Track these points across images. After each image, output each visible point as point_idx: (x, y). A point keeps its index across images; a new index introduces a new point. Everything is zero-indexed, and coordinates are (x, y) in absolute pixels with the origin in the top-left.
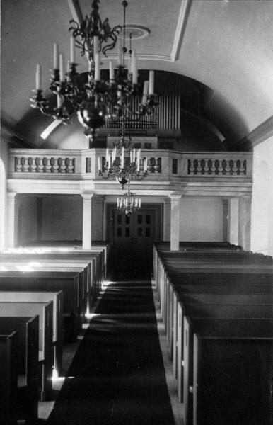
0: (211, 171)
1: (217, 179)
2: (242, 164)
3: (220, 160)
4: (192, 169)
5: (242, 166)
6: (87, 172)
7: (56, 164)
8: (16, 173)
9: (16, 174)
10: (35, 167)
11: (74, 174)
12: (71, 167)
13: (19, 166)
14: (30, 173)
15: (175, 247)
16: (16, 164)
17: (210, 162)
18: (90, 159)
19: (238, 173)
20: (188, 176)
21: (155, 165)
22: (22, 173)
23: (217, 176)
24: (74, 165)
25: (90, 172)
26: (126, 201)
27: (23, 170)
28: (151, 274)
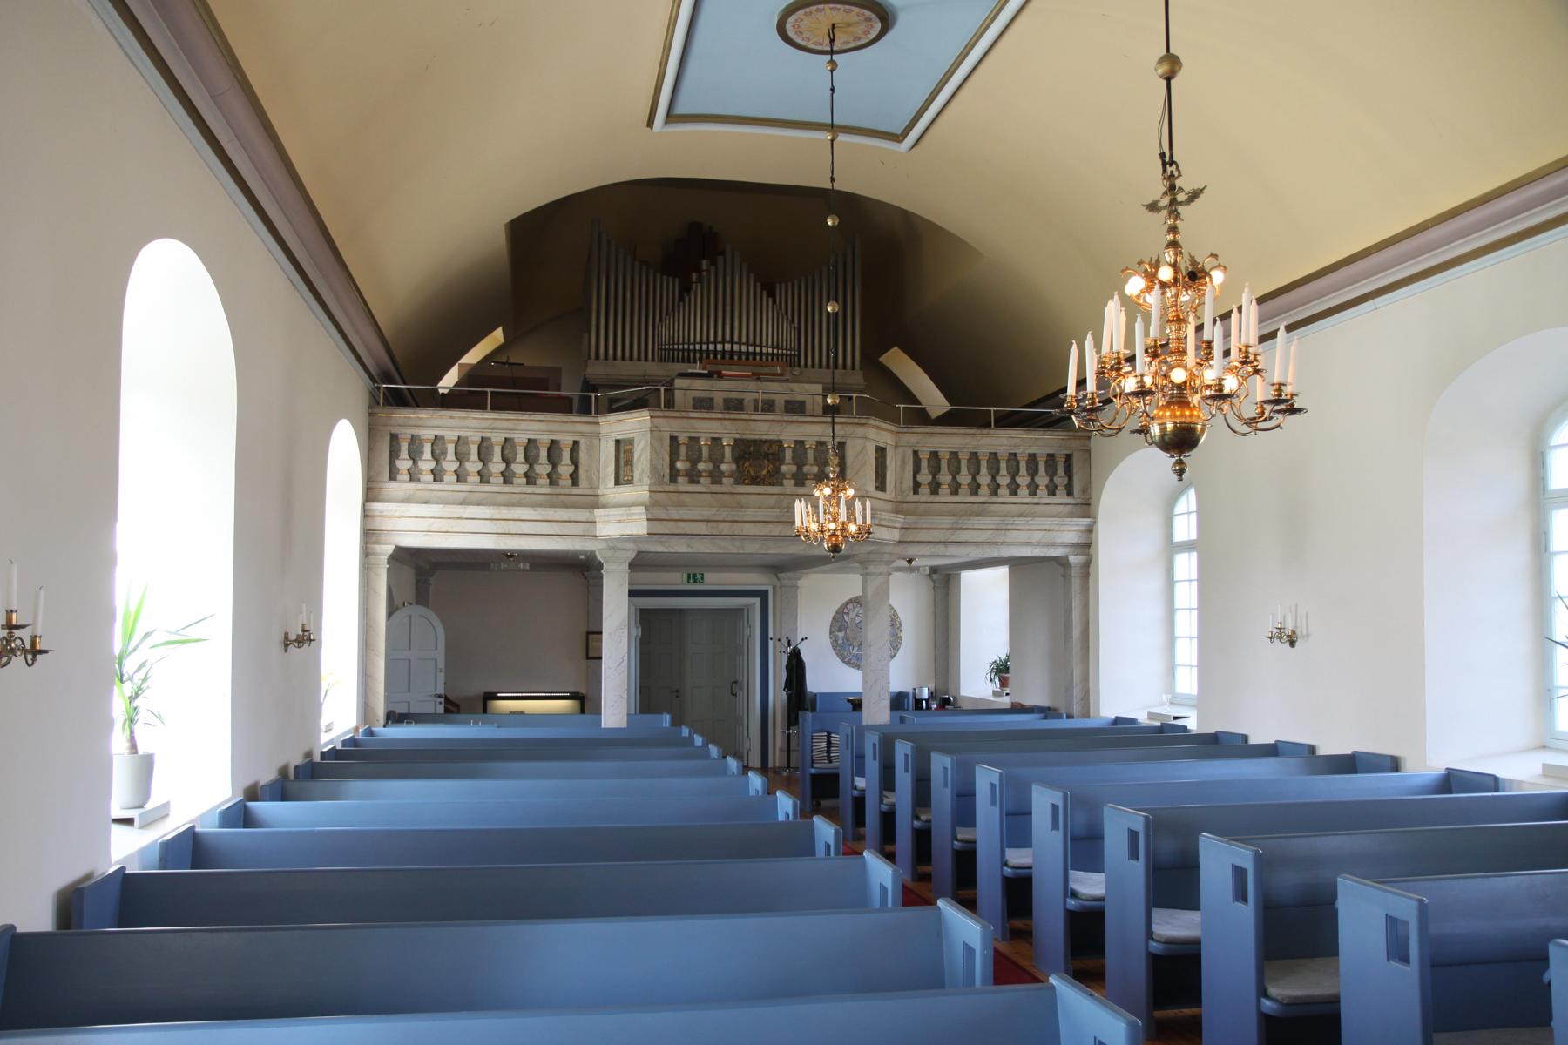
0: (722, 474)
1: (993, 508)
2: (566, 454)
3: (451, 435)
4: (925, 478)
5: (1061, 471)
6: (617, 483)
7: (520, 457)
8: (393, 485)
9: (392, 488)
10: (455, 466)
11: (575, 491)
12: (565, 468)
13: (404, 464)
14: (437, 486)
15: (367, 726)
16: (394, 455)
17: (994, 458)
18: (631, 442)
19: (1052, 491)
20: (916, 498)
21: (699, 460)
22: (412, 485)
23: (994, 499)
24: (575, 461)
25: (630, 482)
26: (502, 566)
27: (413, 476)
28: (1020, 707)
